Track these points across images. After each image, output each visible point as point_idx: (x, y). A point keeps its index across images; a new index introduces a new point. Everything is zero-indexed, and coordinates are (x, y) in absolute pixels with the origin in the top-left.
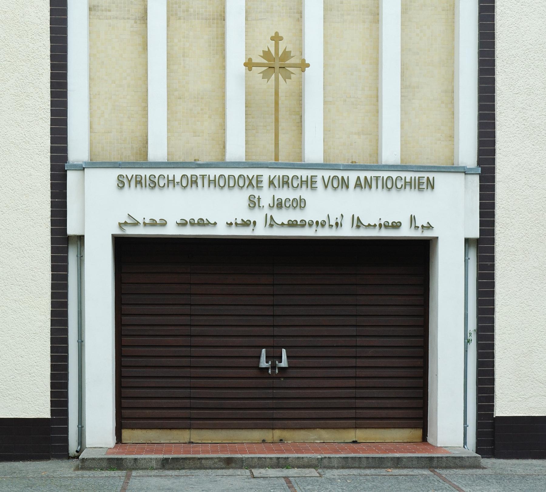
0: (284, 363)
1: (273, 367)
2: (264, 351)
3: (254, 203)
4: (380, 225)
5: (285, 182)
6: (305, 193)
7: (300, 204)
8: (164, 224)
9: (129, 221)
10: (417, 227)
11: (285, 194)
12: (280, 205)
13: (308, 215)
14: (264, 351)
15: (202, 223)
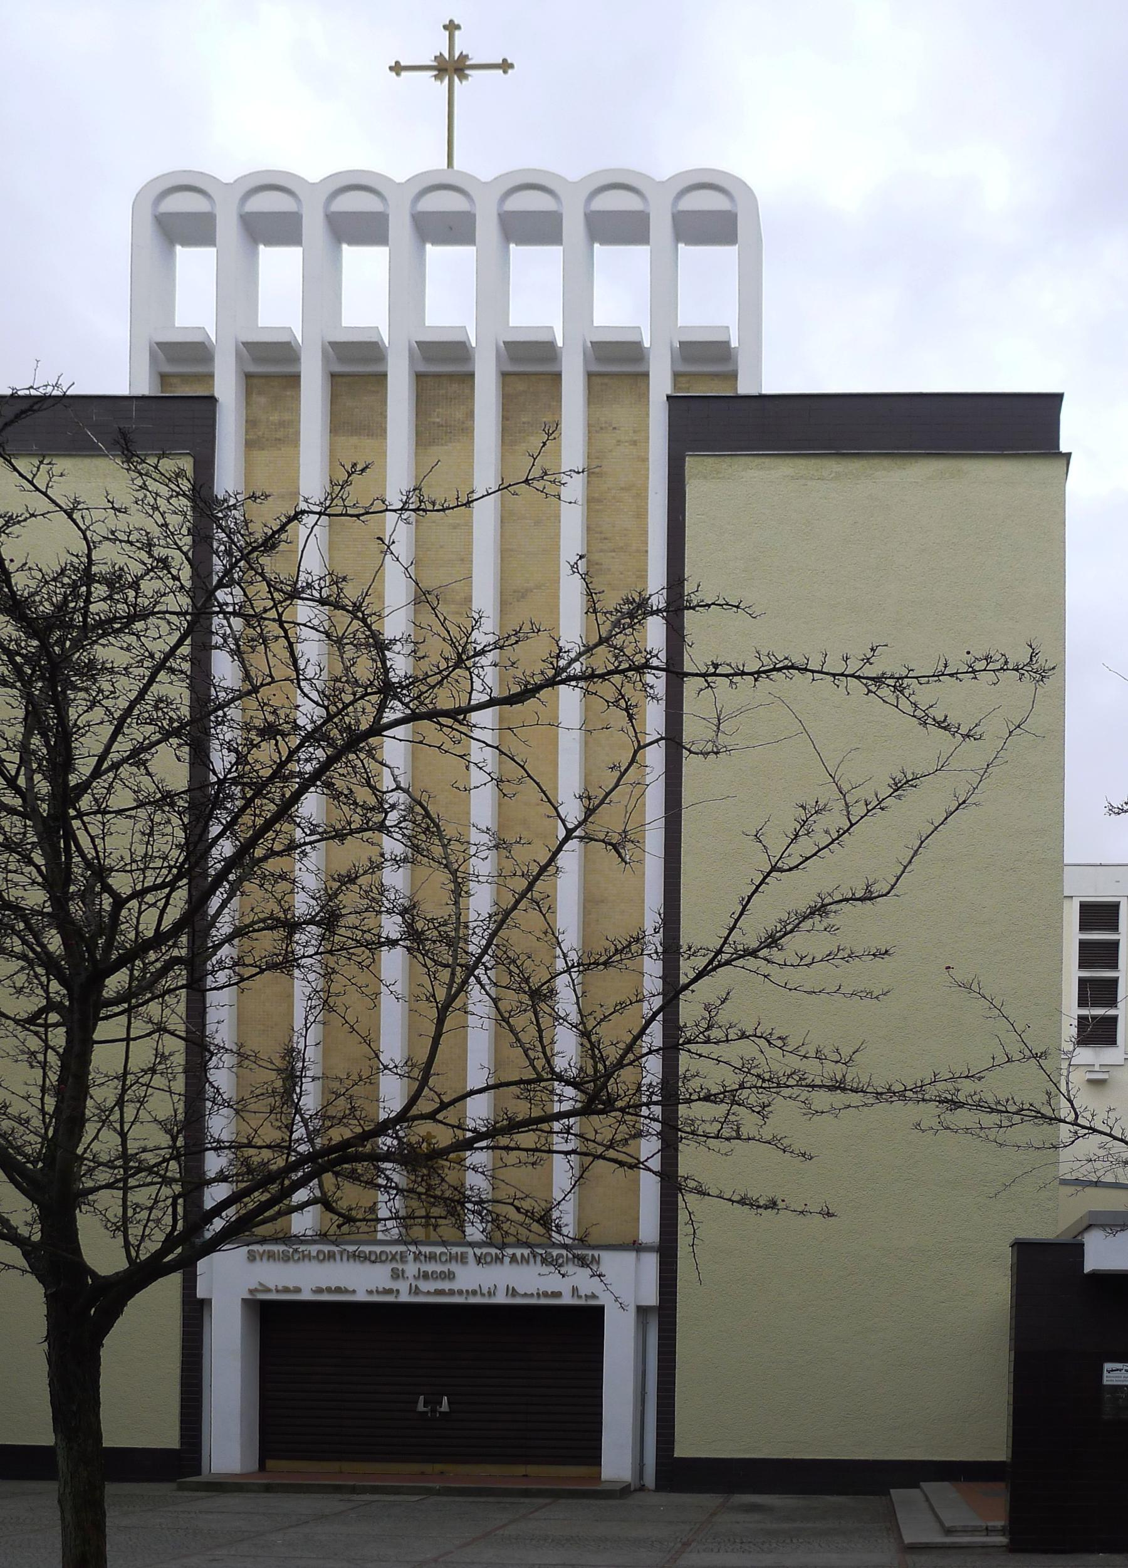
0: (445, 1406)
1: (433, 1411)
2: (422, 1397)
3: (396, 1275)
4: (538, 1294)
5: (432, 1257)
6: (454, 1267)
7: (450, 1276)
8: (298, 1290)
9: (259, 1288)
10: (579, 1297)
11: (430, 1267)
12: (426, 1276)
13: (455, 1286)
14: (422, 1397)
15: (338, 1290)
